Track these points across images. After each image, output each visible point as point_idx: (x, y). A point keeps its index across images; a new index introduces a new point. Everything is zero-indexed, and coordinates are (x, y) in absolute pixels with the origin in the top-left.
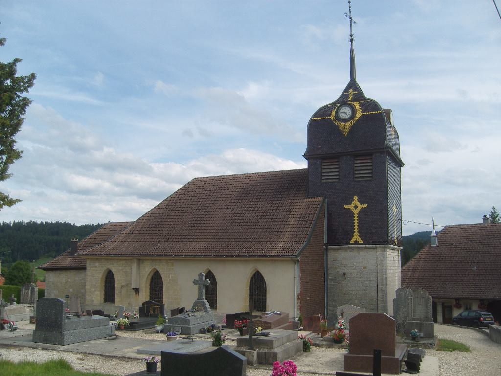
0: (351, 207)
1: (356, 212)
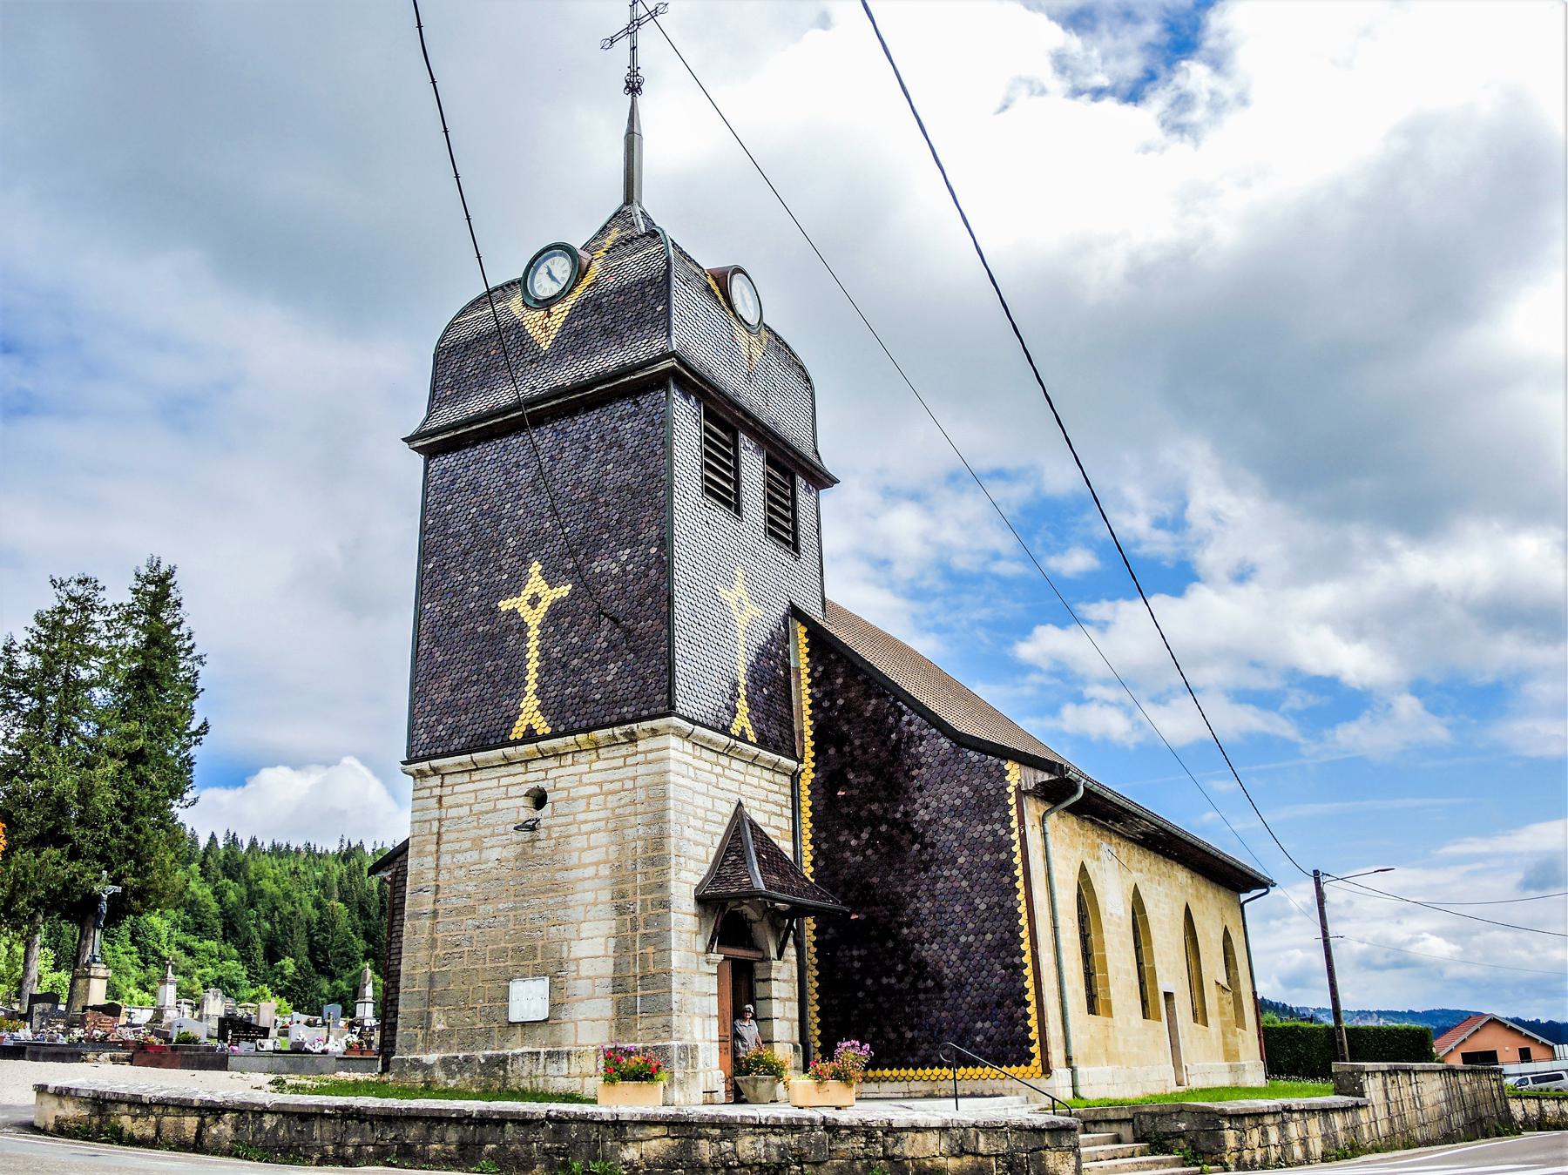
0: (519, 603)
1: (533, 619)
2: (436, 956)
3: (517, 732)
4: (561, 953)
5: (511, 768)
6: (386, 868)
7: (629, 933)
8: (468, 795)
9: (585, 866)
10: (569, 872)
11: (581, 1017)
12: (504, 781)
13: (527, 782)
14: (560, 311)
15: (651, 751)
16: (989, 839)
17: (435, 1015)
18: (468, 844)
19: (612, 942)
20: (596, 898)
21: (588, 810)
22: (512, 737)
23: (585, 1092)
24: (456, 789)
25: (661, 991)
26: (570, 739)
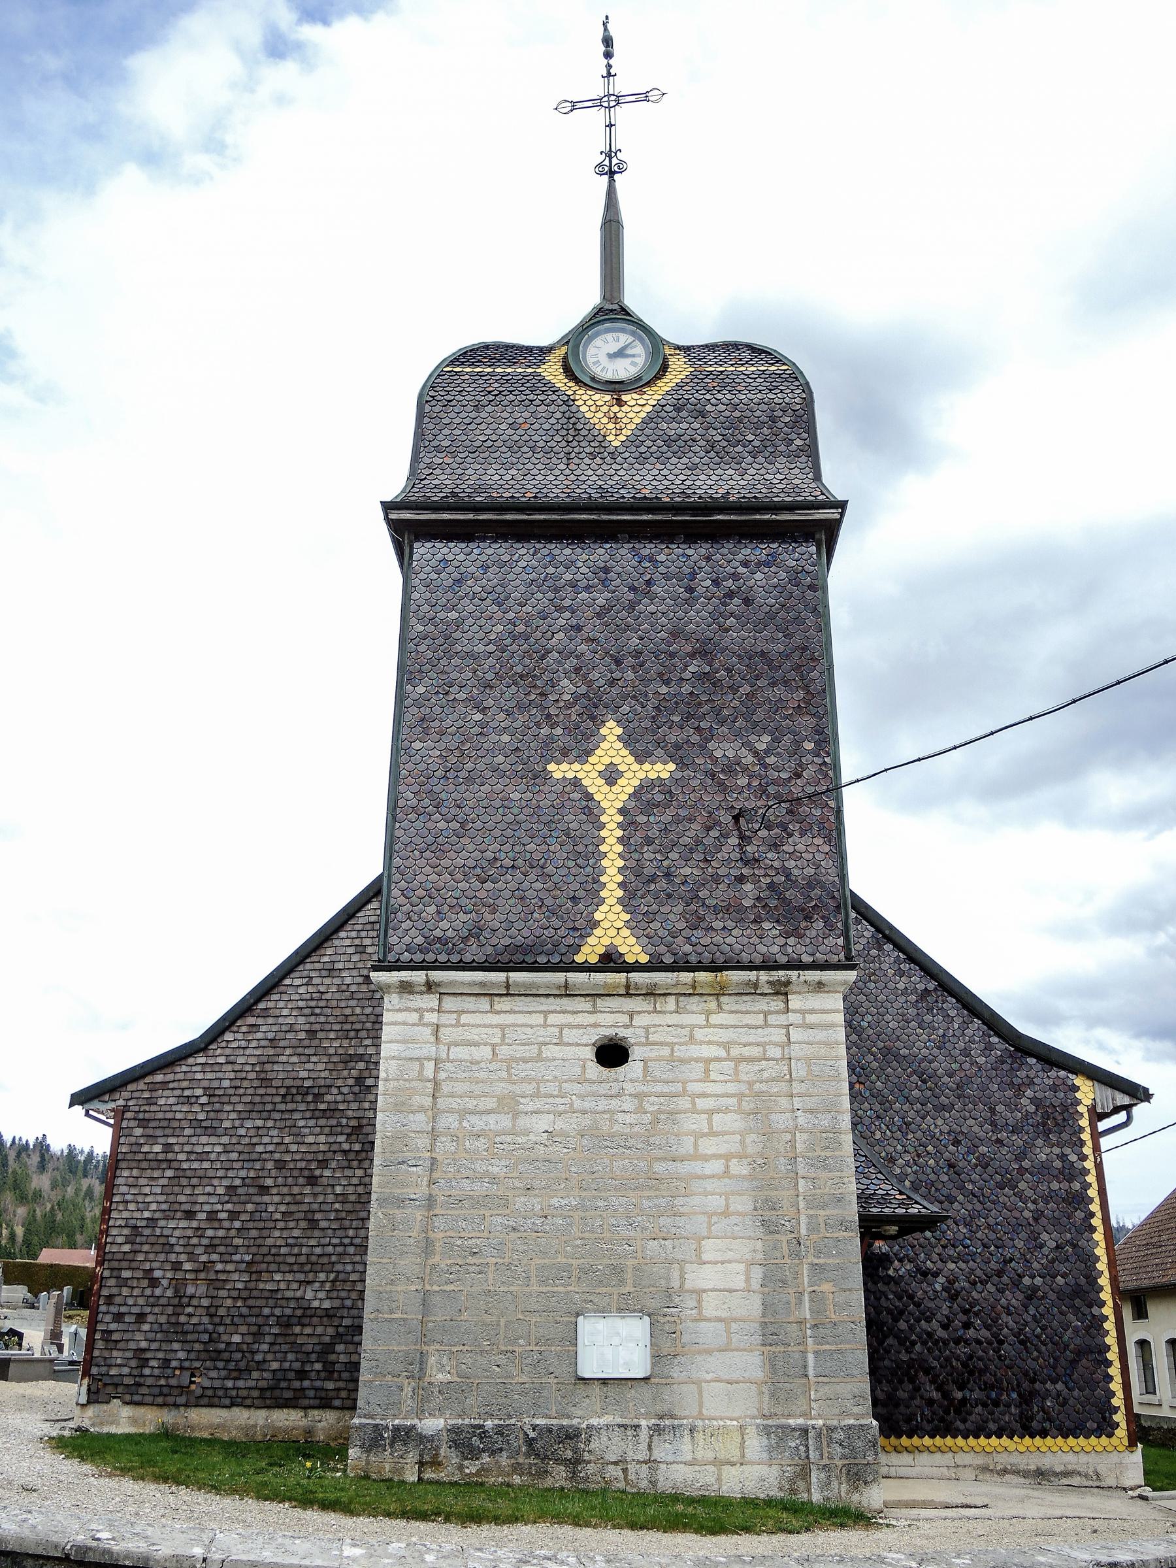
0: (589, 774)
2: (434, 1266)
3: (590, 952)
4: (668, 1279)
5: (565, 1001)
6: (107, 1097)
7: (786, 1260)
8: (490, 1031)
9: (706, 1158)
10: (679, 1164)
11: (709, 1377)
12: (553, 1019)
13: (596, 1025)
14: (637, 407)
15: (812, 1011)
16: (1058, 1164)
17: (432, 1360)
18: (491, 1103)
19: (757, 1273)
20: (727, 1206)
21: (706, 1078)
22: (579, 958)
23: (724, 1488)
24: (464, 1019)
25: (847, 1346)
26: (686, 977)
